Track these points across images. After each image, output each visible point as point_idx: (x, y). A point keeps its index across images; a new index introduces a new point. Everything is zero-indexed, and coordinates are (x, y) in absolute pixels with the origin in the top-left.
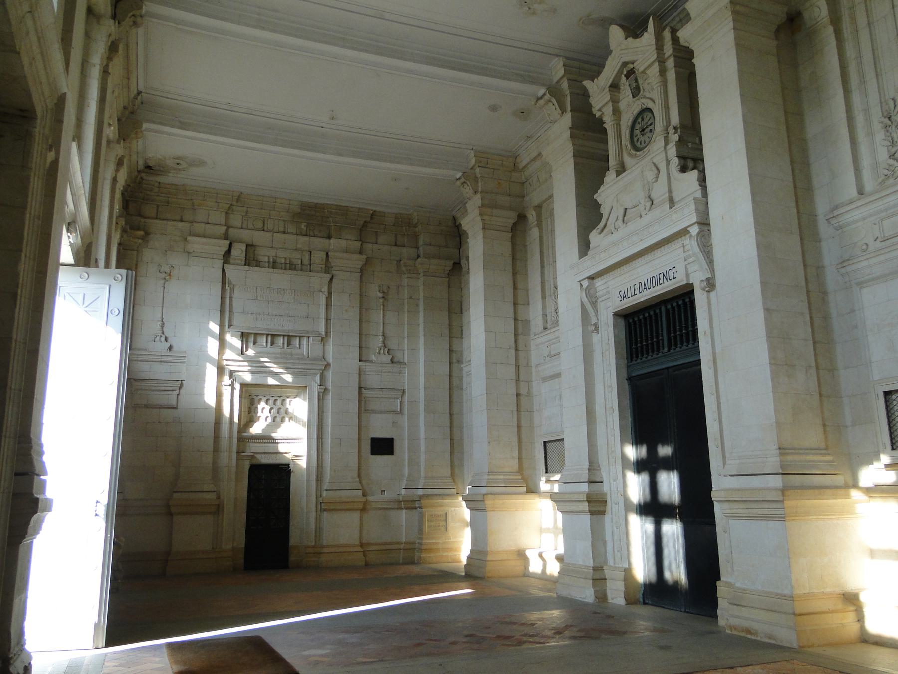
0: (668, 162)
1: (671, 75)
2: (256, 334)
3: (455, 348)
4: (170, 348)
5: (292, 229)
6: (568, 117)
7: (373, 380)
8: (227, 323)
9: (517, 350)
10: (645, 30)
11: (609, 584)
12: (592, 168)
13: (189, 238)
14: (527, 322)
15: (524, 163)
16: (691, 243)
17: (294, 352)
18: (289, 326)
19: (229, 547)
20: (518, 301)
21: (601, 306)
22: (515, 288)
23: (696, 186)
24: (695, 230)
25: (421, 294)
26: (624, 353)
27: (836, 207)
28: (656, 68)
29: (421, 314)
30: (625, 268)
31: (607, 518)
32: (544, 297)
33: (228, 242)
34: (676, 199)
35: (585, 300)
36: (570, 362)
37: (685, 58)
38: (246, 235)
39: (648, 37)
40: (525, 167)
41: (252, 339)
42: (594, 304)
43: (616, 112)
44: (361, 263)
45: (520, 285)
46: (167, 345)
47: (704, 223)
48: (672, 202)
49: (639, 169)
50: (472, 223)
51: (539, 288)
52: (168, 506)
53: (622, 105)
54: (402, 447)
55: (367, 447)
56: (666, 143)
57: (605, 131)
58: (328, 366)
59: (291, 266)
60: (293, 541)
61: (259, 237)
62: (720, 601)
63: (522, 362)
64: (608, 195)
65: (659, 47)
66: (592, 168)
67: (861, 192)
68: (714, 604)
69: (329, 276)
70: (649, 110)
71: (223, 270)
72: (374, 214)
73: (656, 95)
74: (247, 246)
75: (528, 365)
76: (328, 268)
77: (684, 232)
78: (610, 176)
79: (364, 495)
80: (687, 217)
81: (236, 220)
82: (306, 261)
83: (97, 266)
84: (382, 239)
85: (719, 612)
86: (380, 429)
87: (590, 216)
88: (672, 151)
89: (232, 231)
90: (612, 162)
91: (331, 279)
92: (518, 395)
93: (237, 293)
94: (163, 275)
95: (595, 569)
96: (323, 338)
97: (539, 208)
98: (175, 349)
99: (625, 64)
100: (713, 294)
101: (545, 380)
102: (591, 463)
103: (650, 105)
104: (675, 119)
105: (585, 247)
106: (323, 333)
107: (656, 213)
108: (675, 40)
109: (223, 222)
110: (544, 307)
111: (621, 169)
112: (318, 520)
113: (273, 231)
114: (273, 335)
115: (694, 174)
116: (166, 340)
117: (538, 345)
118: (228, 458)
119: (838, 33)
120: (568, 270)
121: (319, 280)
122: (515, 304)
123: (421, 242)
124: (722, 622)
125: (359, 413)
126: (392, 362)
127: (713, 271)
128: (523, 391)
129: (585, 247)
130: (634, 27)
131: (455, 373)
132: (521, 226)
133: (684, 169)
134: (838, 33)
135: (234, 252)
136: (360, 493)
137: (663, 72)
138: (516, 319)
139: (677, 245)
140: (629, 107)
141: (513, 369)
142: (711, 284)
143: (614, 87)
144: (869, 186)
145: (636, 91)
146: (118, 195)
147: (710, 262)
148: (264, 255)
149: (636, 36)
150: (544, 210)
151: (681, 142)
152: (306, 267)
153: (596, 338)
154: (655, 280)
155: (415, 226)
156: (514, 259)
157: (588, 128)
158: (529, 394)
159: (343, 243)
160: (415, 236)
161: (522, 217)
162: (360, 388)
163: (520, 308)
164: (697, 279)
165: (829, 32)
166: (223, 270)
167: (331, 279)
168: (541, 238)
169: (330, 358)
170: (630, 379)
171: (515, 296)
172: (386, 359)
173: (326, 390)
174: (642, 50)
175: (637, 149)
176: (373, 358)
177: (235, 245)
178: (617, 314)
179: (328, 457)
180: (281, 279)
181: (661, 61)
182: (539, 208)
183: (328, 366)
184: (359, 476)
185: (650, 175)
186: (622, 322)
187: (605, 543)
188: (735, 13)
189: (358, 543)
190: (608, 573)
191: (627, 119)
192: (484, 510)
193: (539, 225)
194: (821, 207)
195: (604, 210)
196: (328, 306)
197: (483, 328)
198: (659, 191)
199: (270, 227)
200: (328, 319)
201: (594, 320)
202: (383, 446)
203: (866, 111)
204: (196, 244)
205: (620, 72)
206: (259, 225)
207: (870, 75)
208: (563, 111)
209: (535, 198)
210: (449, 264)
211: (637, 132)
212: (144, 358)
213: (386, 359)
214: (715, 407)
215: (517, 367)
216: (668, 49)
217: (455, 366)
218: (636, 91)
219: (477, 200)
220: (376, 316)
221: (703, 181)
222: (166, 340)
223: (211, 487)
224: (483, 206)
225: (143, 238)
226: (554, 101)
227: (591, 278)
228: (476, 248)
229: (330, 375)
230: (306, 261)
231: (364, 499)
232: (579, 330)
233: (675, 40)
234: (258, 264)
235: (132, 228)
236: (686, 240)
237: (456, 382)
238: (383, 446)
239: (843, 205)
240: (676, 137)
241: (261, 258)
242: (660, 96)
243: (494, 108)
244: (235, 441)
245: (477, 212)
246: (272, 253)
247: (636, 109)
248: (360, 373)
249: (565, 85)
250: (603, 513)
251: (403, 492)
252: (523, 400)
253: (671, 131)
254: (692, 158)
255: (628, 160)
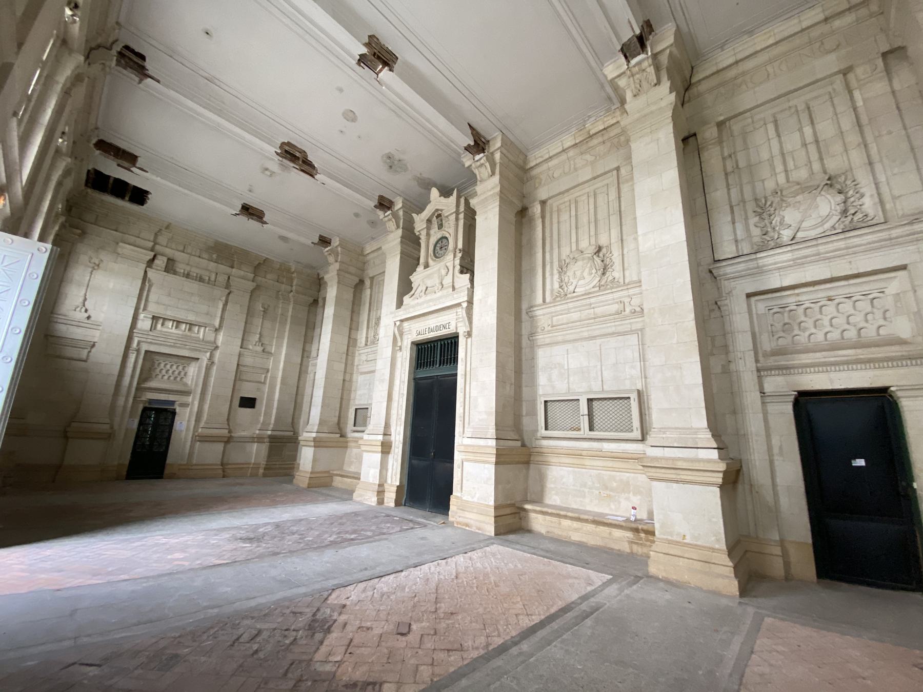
0: (454, 267)
1: (461, 222)
2: (164, 319)
3: (307, 349)
4: (89, 318)
5: (205, 255)
6: (496, 179)
7: (248, 360)
8: (142, 306)
9: (347, 354)
10: (452, 194)
11: (386, 494)
12: (410, 263)
13: (121, 244)
14: (356, 340)
15: (532, 164)
16: (461, 312)
17: (193, 335)
18: (191, 318)
19: (116, 463)
20: (353, 326)
21: (405, 337)
22: (352, 320)
23: (467, 283)
24: (465, 305)
25: (290, 313)
26: (414, 364)
27: (532, 307)
28: (454, 216)
29: (288, 327)
30: (436, 315)
31: (391, 456)
32: (368, 328)
33: (153, 254)
34: (456, 287)
35: (396, 332)
36: (382, 366)
37: (470, 216)
38: (168, 251)
39: (453, 199)
40: (700, 81)
41: (161, 321)
42: (401, 334)
43: (428, 235)
44: (252, 288)
45: (355, 318)
46: (86, 315)
47: (470, 302)
48: (454, 288)
49: (436, 267)
50: (331, 278)
51: (366, 323)
52: (65, 432)
53: (432, 232)
54: (261, 406)
55: (237, 402)
56: (455, 257)
57: (419, 245)
58: (217, 347)
59: (201, 280)
60: (170, 460)
61: (178, 256)
62: (451, 507)
63: (349, 362)
64: (418, 277)
65: (458, 206)
66: (410, 263)
67: (544, 301)
68: (447, 507)
69: (227, 291)
70: (446, 238)
71: (146, 272)
72: (266, 260)
73: (452, 231)
74: (169, 259)
75: (353, 364)
76: (228, 286)
77: (459, 305)
78: (420, 269)
79: (230, 432)
80: (463, 297)
81: (162, 240)
82: (213, 278)
83: (27, 235)
84: (269, 276)
85: (450, 513)
86: (247, 391)
87: (405, 287)
88: (457, 262)
89: (158, 247)
90: (422, 260)
91: (229, 294)
92: (344, 380)
93: (153, 289)
94: (92, 265)
95: (379, 485)
96: (216, 330)
97: (372, 278)
98: (92, 319)
99: (437, 210)
100: (469, 340)
101: (362, 373)
102: (386, 424)
103: (447, 235)
104: (460, 246)
105: (400, 304)
106: (217, 326)
107: (444, 292)
108: (467, 203)
109: (152, 239)
110: (367, 334)
111: (427, 266)
112: (192, 446)
113: (191, 254)
114: (178, 322)
115: (468, 276)
116: (86, 311)
117: (361, 355)
118: (125, 401)
119: (543, 222)
120: (388, 315)
121: (220, 293)
122: (350, 329)
123: (295, 283)
124: (451, 519)
125: (235, 381)
126: (263, 351)
127: (471, 328)
128: (347, 378)
129: (400, 304)
130: (445, 192)
131: (304, 363)
132: (360, 287)
133: (462, 272)
134: (543, 222)
135: (156, 262)
136: (227, 431)
137: (457, 219)
138: (349, 337)
139: (454, 310)
140: (436, 235)
141: (343, 365)
142: (469, 334)
143: (429, 221)
144: (548, 300)
145: (440, 226)
146: (61, 196)
147: (470, 322)
148: (181, 268)
149: (448, 197)
150: (377, 280)
151: (462, 258)
152: (212, 283)
153: (399, 354)
154: (438, 328)
155: (293, 273)
156: (353, 304)
157: (411, 240)
158: (351, 381)
159: (242, 273)
160: (292, 279)
161: (362, 282)
162: (238, 365)
163: (353, 332)
164: (462, 331)
165: (539, 223)
166: (146, 272)
167: (229, 294)
168: (371, 295)
169: (219, 343)
170: (415, 379)
171: (351, 324)
172: (259, 349)
173: (213, 363)
174: (448, 205)
175: (436, 257)
176: (251, 347)
177: (159, 257)
178: (413, 343)
179: (206, 407)
180: (193, 286)
181: (457, 213)
182: (372, 278)
183: (217, 347)
184: (228, 420)
185: (443, 272)
186: (415, 348)
187: (387, 470)
188: (501, 198)
189: (219, 463)
190: (386, 486)
191: (433, 240)
192: (158, 420)
193: (371, 288)
194: (524, 306)
195: (414, 285)
196: (224, 310)
197: (329, 339)
198: (448, 281)
199: (189, 251)
200: (222, 318)
201: (399, 344)
202: (248, 403)
203: (552, 263)
204: (126, 249)
205: (433, 214)
206: (182, 248)
207: (124, 390)
208: (398, 227)
209: (371, 272)
210: (311, 300)
211: (438, 248)
212: (65, 322)
213: (259, 349)
214: (462, 400)
215: (346, 364)
216: (462, 208)
217: (305, 359)
218: (440, 226)
219: (337, 266)
220: (258, 321)
221: (472, 281)
222: (86, 311)
223: (107, 421)
224: (339, 270)
225: (80, 235)
226: (487, 165)
227: (402, 321)
228: (331, 293)
229: (217, 354)
230: (213, 278)
231: (228, 435)
232: (390, 349)
233: (467, 203)
234: (175, 273)
235: (71, 226)
236: (459, 310)
237: (303, 368)
238: (248, 403)
239: (536, 306)
240: (460, 255)
241: (178, 270)
242: (454, 232)
243: (357, 215)
244: (133, 390)
245: (335, 273)
246: (188, 268)
247: (439, 236)
248: (240, 355)
249: (401, 213)
250: (388, 453)
251: (257, 432)
252: (347, 384)
253: (458, 251)
254: (467, 267)
255: (431, 262)
